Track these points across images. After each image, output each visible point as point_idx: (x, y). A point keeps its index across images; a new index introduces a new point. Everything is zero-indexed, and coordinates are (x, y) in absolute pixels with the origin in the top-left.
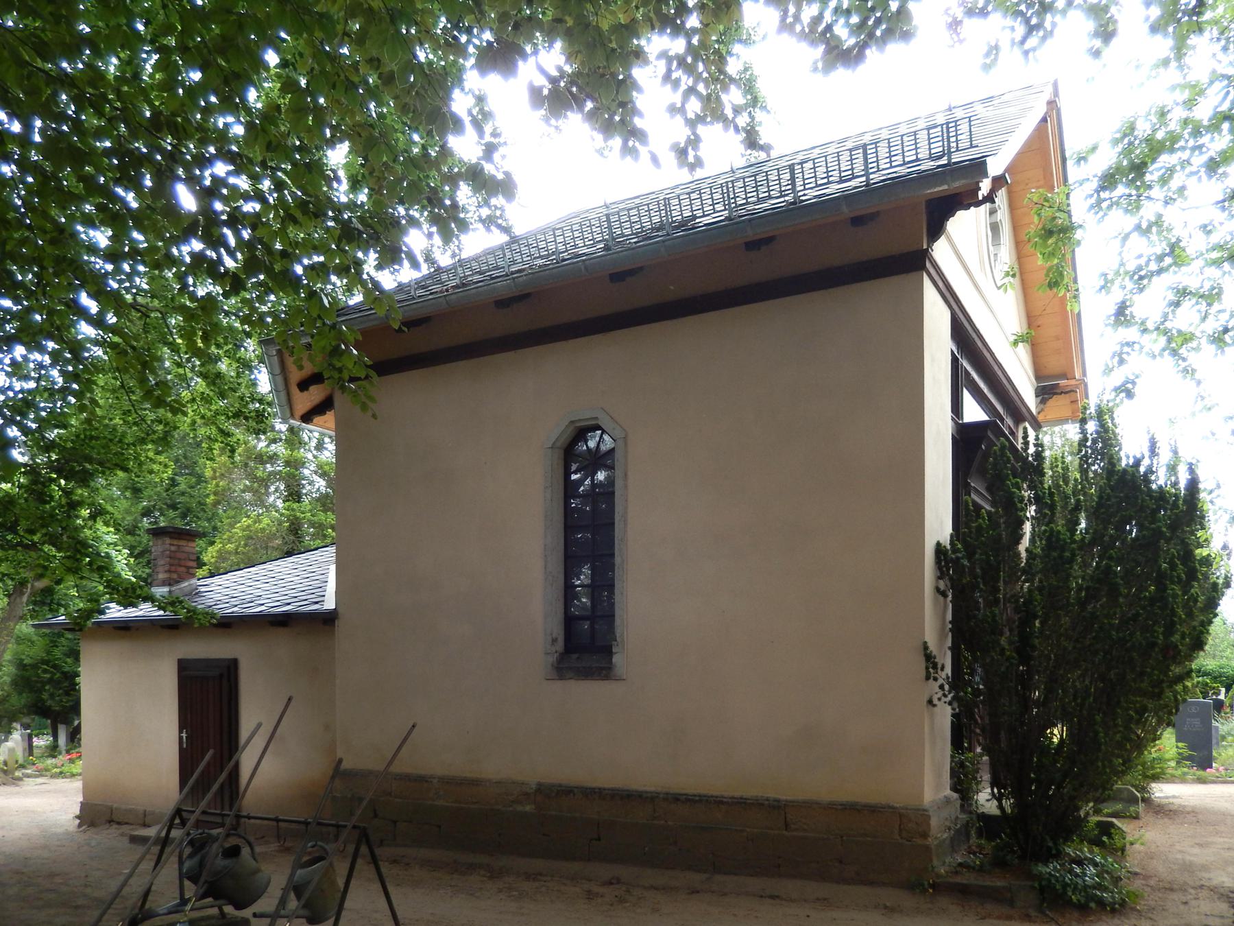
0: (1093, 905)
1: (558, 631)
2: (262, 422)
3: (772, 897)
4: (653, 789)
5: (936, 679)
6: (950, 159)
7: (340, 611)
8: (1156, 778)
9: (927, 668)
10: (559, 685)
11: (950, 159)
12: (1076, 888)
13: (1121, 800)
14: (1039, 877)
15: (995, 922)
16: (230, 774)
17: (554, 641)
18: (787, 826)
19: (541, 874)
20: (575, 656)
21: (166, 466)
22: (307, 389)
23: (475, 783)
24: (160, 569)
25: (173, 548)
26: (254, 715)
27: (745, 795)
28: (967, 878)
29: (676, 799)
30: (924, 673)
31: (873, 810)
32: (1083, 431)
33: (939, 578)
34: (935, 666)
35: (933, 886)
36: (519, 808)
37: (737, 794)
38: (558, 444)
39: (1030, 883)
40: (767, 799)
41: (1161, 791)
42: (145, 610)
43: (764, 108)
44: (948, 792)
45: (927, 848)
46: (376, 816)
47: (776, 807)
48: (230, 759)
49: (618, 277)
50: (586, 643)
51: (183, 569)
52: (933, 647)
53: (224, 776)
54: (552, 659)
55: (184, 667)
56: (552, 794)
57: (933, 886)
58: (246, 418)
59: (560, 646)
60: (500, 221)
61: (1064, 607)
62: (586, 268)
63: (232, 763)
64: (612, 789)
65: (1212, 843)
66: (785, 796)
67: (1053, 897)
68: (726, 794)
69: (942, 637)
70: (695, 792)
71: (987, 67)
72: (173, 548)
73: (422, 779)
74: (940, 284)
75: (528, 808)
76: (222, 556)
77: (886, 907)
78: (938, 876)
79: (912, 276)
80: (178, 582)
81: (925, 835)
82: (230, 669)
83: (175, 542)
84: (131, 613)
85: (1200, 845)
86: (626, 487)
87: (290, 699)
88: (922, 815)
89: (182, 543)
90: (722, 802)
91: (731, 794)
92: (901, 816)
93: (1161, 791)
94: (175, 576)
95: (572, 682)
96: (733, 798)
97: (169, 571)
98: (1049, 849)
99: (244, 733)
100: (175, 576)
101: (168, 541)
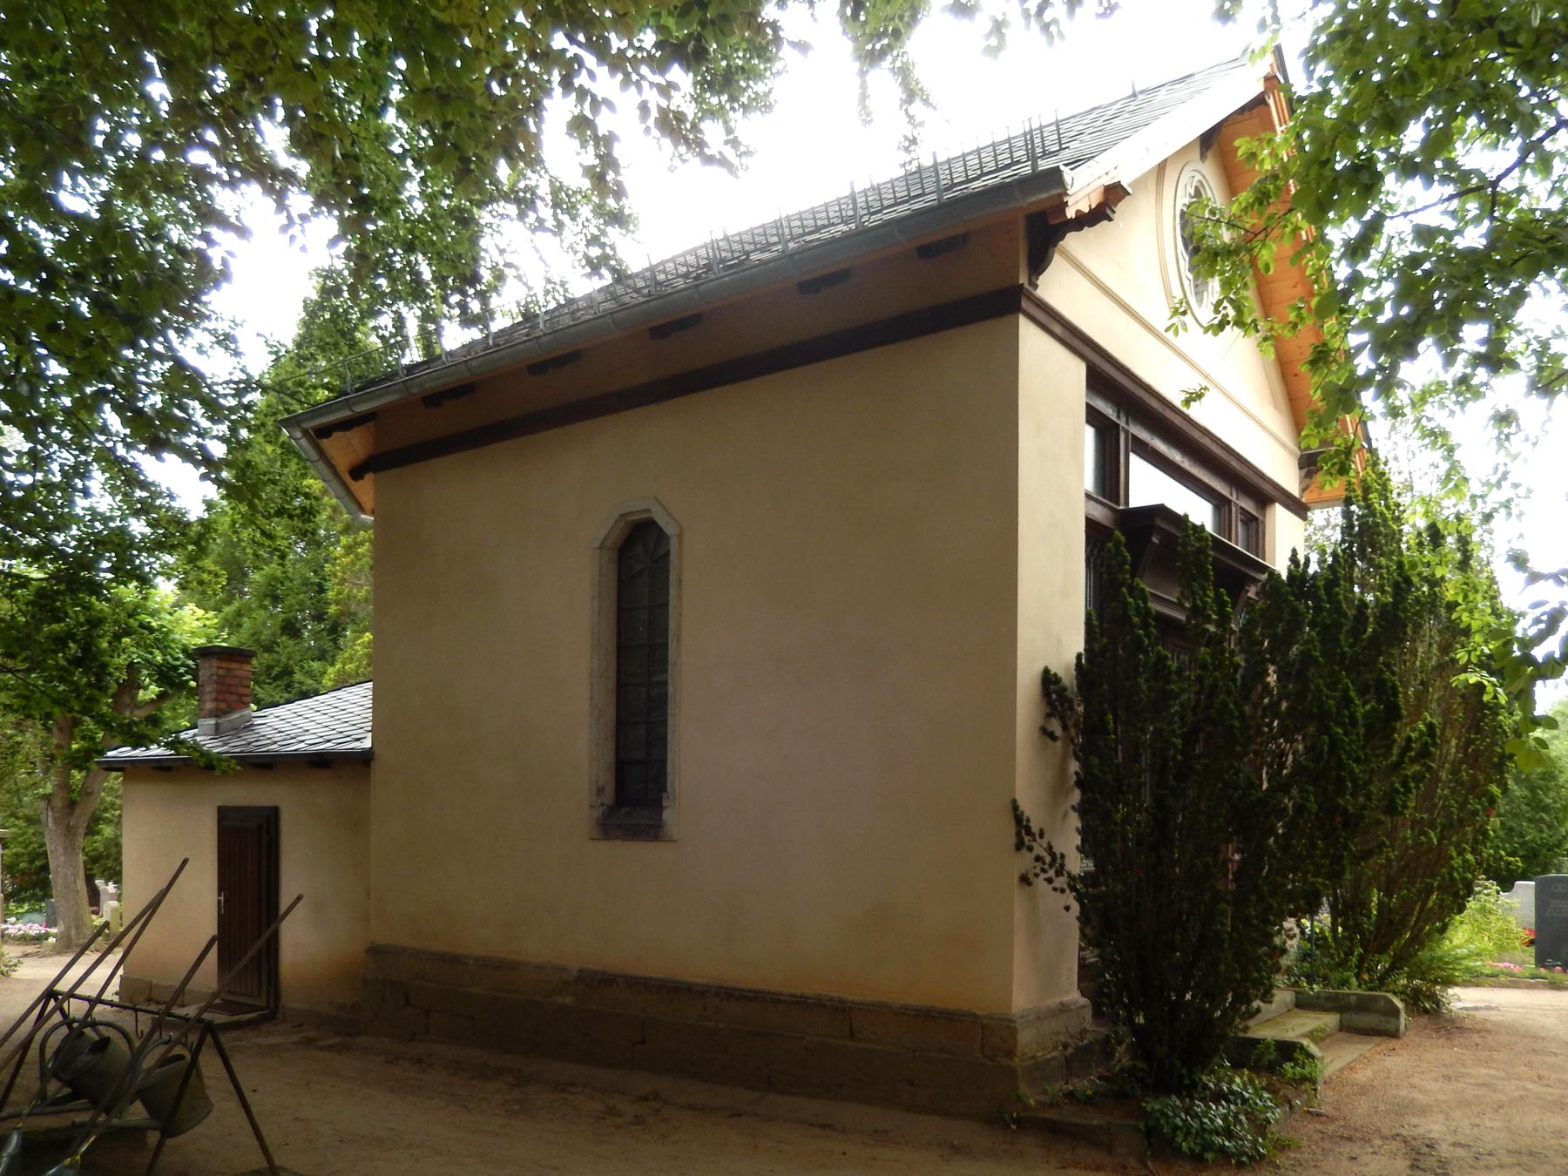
0: (1209, 1156)
1: (608, 780)
2: (309, 521)
3: (824, 1126)
4: (704, 981)
5: (1030, 849)
6: (1034, 165)
7: (377, 751)
8: (1449, 982)
9: (1018, 834)
10: (605, 848)
11: (1034, 165)
12: (1188, 1133)
13: (1377, 1011)
14: (1146, 1115)
15: (1083, 1173)
16: (268, 941)
17: (600, 790)
18: (852, 1036)
19: (572, 1084)
20: (625, 810)
21: (217, 575)
22: (362, 478)
23: (512, 966)
24: (207, 697)
25: (221, 672)
26: (300, 873)
27: (808, 992)
28: (1069, 1115)
29: (730, 994)
30: (1013, 840)
31: (951, 1018)
32: (1347, 515)
33: (1049, 716)
34: (1029, 831)
35: (1018, 1121)
36: (560, 1000)
37: (798, 992)
38: (609, 543)
39: (1132, 1122)
40: (831, 999)
41: (1461, 999)
42: (155, 751)
43: (926, 102)
44: (1074, 996)
45: (1013, 1071)
46: (408, 1003)
47: (840, 1011)
48: (269, 925)
49: (661, 331)
50: (636, 790)
51: (233, 697)
52: (1027, 808)
53: (260, 943)
54: (597, 813)
55: (224, 814)
56: (597, 982)
57: (1018, 1121)
58: (291, 517)
59: (609, 796)
60: (613, 263)
61: (1268, 752)
62: (614, 322)
63: (267, 934)
64: (660, 980)
65: (1463, 1075)
66: (852, 996)
67: (1159, 1142)
68: (785, 991)
69: (1058, 790)
70: (751, 986)
71: (992, 51)
72: (221, 672)
73: (456, 960)
74: (1057, 329)
75: (568, 1000)
76: (341, 673)
77: (953, 1147)
78: (1026, 1107)
79: (1006, 320)
80: (225, 713)
81: (1010, 1053)
82: (271, 817)
83: (224, 665)
84: (140, 753)
85: (1448, 1078)
86: (680, 597)
87: (185, 862)
88: (1007, 1027)
89: (234, 666)
90: (779, 1001)
91: (793, 991)
92: (983, 1027)
93: (1461, 999)
94: (223, 706)
95: (618, 842)
96: (792, 995)
97: (216, 700)
98: (1181, 1077)
99: (285, 901)
100: (223, 706)
101: (215, 663)
